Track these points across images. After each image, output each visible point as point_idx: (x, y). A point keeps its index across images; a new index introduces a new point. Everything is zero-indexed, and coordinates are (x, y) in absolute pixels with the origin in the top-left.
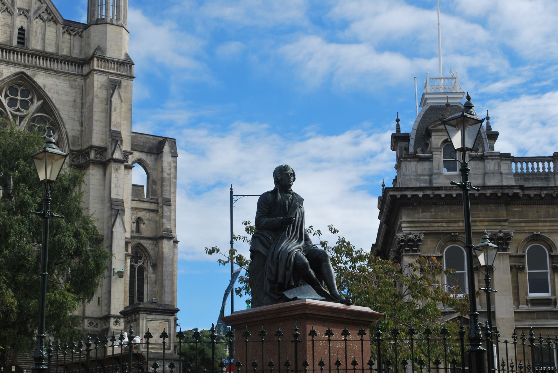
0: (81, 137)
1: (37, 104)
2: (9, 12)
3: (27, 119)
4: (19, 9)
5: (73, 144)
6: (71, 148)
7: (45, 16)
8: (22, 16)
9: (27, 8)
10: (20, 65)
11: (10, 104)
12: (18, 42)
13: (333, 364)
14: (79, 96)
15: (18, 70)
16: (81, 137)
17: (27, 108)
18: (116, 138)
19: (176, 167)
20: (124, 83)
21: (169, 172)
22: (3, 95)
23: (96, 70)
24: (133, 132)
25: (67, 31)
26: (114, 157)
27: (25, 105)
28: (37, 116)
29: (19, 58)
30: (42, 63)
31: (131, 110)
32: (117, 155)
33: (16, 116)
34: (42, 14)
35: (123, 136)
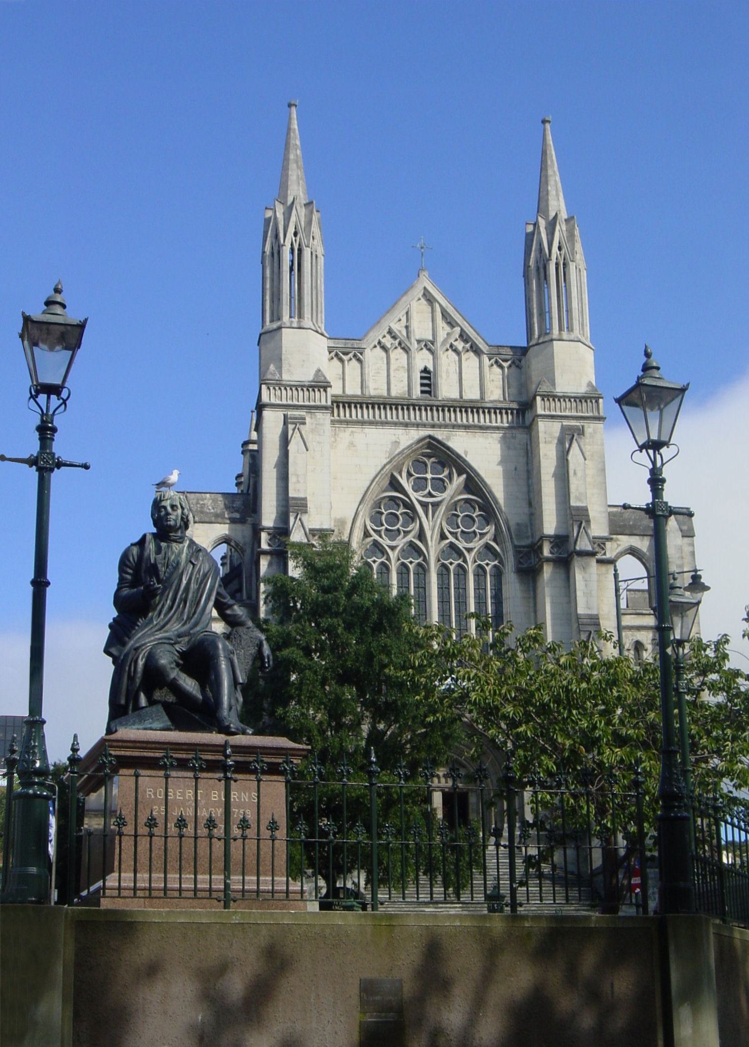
0: (531, 524)
1: (459, 481)
2: (403, 349)
3: (442, 508)
4: (419, 341)
5: (519, 536)
6: (516, 543)
7: (460, 345)
8: (425, 351)
9: (431, 338)
10: (424, 425)
11: (416, 488)
12: (422, 392)
13: (171, 825)
14: (523, 460)
15: (424, 432)
16: (531, 524)
17: (444, 489)
18: (575, 517)
19: (693, 554)
20: (590, 428)
21: (679, 562)
22: (404, 474)
23: (541, 416)
24: (610, 506)
25: (496, 362)
26: (578, 548)
27: (440, 485)
28: (385, 497)
29: (425, 416)
30: (461, 418)
31: (603, 470)
32: (584, 545)
33: (428, 503)
34: (455, 343)
35: (592, 514)
